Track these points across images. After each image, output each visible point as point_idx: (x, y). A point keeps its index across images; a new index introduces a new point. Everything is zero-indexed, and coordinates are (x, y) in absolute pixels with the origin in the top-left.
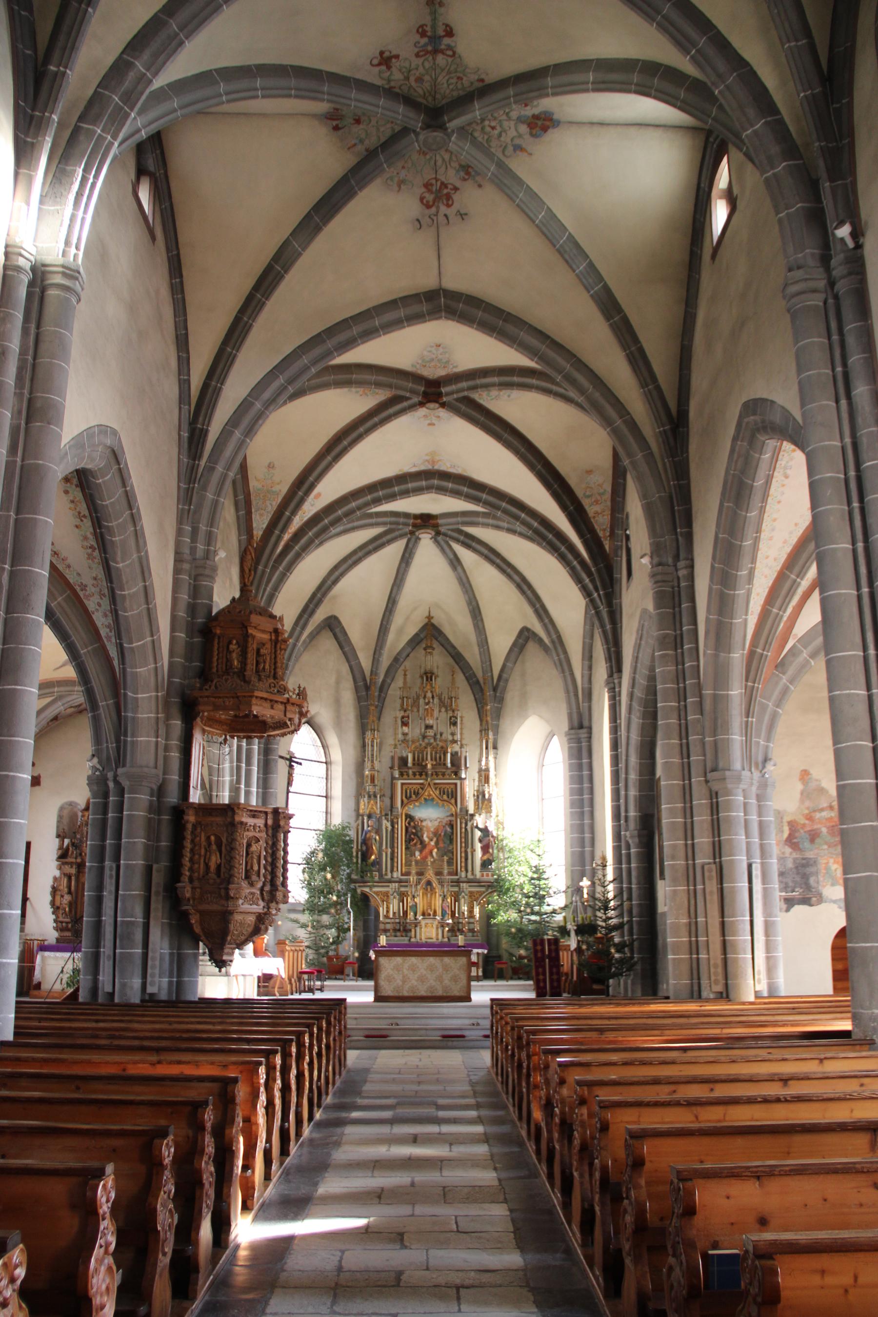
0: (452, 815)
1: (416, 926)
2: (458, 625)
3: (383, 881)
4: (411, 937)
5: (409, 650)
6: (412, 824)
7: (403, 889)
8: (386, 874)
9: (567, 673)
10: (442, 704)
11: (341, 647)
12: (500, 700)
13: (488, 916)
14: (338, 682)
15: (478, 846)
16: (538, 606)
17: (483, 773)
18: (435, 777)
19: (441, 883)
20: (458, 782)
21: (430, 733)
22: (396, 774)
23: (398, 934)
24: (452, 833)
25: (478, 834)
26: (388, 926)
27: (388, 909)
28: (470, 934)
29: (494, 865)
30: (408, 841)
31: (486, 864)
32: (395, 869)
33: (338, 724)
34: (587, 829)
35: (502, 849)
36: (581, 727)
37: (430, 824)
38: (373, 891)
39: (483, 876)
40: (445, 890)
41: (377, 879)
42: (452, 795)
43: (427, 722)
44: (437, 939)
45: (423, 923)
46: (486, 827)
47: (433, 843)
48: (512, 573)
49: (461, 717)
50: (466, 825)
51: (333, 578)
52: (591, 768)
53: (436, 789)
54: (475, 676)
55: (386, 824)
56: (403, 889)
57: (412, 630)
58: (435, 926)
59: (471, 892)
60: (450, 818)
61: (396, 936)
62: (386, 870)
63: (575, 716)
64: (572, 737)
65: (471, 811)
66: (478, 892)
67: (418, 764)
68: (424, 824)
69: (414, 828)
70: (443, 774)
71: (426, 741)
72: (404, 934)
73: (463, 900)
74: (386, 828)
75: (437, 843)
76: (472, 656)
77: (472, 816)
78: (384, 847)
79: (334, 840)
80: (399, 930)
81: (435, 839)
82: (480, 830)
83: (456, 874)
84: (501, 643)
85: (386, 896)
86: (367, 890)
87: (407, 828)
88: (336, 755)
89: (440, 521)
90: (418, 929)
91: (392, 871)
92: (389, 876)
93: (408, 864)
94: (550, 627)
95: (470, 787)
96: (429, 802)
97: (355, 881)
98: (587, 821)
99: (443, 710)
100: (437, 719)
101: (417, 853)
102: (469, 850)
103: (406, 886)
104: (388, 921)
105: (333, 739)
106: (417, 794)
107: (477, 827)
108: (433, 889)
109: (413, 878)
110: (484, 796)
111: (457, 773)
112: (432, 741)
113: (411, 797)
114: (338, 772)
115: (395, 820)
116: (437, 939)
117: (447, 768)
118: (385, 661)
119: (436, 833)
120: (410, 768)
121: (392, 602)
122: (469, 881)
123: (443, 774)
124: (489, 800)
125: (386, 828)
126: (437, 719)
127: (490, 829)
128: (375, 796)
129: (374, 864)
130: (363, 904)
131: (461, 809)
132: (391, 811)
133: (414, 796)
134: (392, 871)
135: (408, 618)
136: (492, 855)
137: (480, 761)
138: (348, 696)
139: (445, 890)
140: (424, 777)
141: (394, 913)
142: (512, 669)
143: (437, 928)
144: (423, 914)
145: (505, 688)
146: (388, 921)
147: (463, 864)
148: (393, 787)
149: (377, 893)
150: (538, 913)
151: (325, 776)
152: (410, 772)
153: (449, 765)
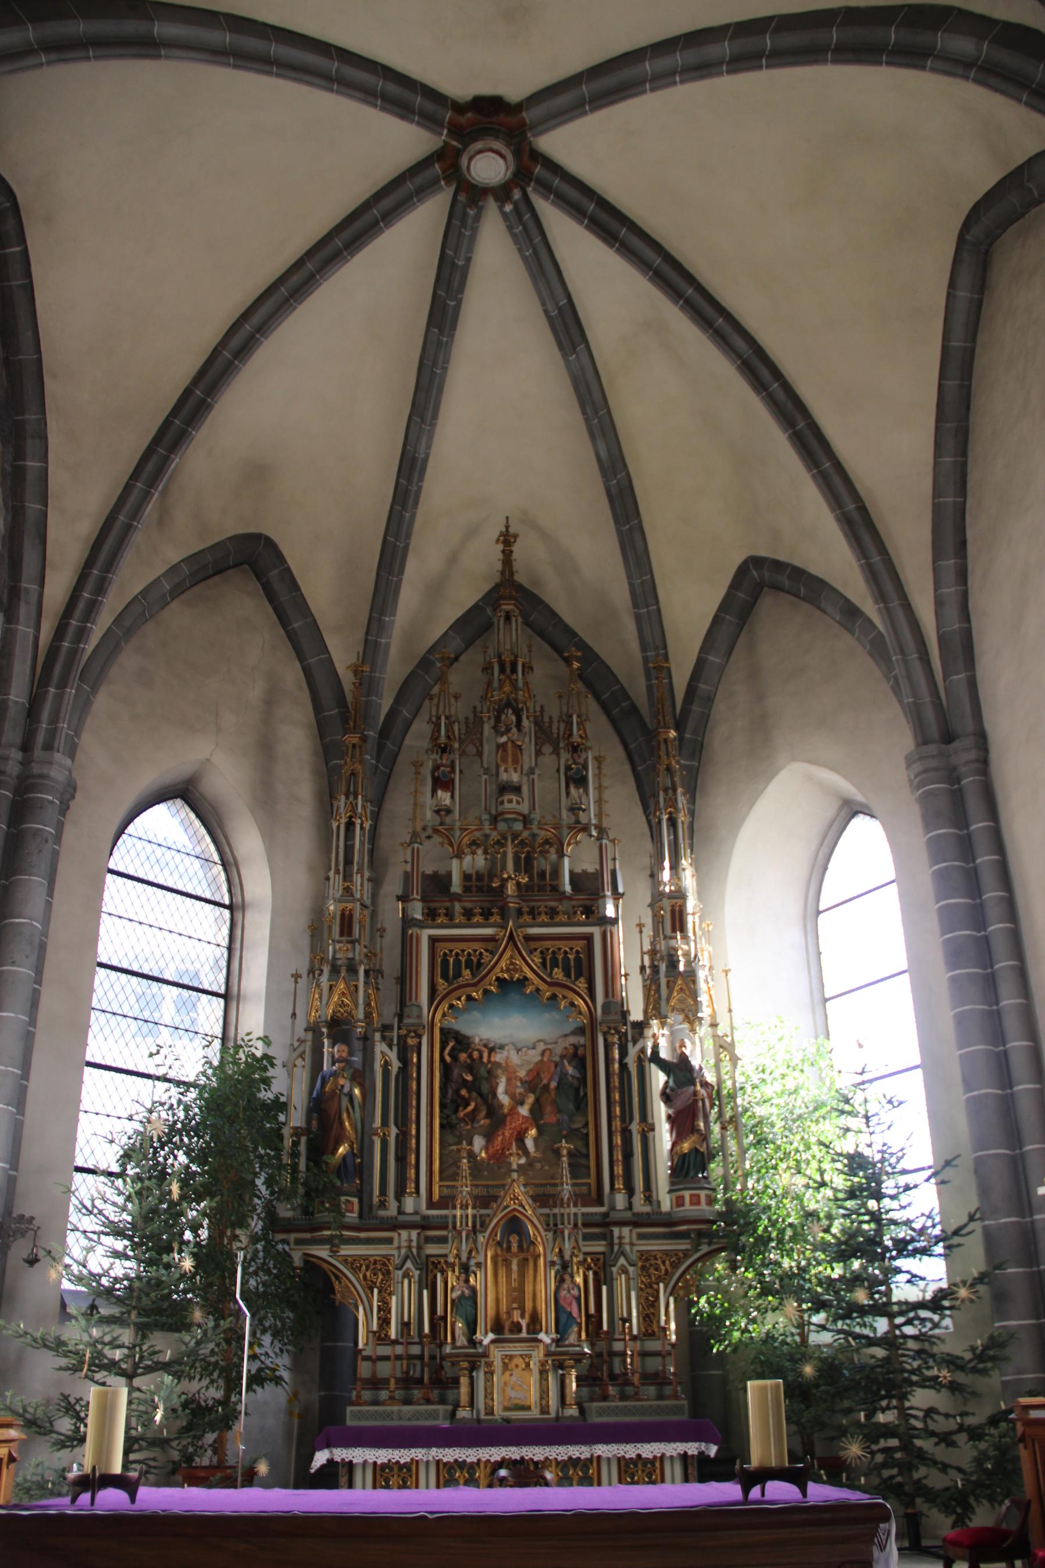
0: (580, 1031)
1: (473, 1367)
2: (578, 571)
3: (372, 1222)
4: (457, 1405)
5: (457, 643)
6: (463, 1056)
7: (432, 1250)
8: (383, 1205)
9: (895, 603)
10: (544, 735)
11: (284, 620)
12: (695, 749)
13: (699, 1334)
14: (270, 701)
15: (661, 1111)
16: (801, 425)
17: (666, 903)
18: (527, 918)
19: (553, 1226)
20: (596, 931)
21: (512, 804)
22: (417, 911)
23: (417, 1393)
24: (583, 1080)
25: (659, 1079)
26: (384, 1369)
27: (382, 1314)
28: (652, 1390)
29: (715, 1168)
30: (451, 1105)
31: (689, 1167)
32: (411, 1187)
33: (266, 801)
34: (1012, 1023)
35: (734, 1120)
36: (948, 737)
37: (515, 1059)
38: (343, 1255)
39: (680, 1202)
40: (568, 1246)
41: (352, 1217)
42: (581, 966)
43: (504, 777)
44: (544, 1410)
45: (496, 1355)
46: (684, 1060)
47: (524, 1111)
48: (728, 330)
49: (599, 759)
50: (624, 1053)
51: (236, 342)
52: (999, 845)
53: (531, 952)
54: (628, 697)
55: (384, 1053)
56: (432, 1250)
57: (464, 596)
58: (534, 1366)
59: (646, 1257)
60: (573, 1040)
61: (407, 1402)
62: (383, 1192)
63: (929, 714)
64: (934, 763)
65: (636, 1014)
66: (666, 1253)
67: (480, 889)
68: (498, 1057)
69: (470, 1068)
70: (553, 913)
71: (502, 826)
72: (435, 1394)
73: (621, 1283)
74: (386, 1065)
75: (537, 1111)
76: (621, 650)
77: (640, 1027)
78: (378, 1122)
79: (232, 1108)
80: (420, 1381)
81: (531, 1099)
82: (664, 1065)
83: (600, 1202)
84: (691, 605)
85: (379, 1276)
86: (322, 1252)
87: (446, 1069)
88: (258, 884)
89: (528, 116)
90: (480, 1376)
91: (400, 1194)
92: (392, 1210)
93: (449, 1171)
94: (837, 481)
95: (628, 952)
96: (514, 996)
97: (288, 1227)
98: (1009, 1001)
99: (547, 749)
100: (532, 771)
101: (478, 1142)
102: (635, 1127)
103: (443, 1240)
104: (384, 1350)
105: (249, 842)
106: (475, 966)
107: (655, 1058)
108: (527, 1245)
109: (462, 1214)
110: (673, 964)
111: (592, 913)
112: (518, 826)
113: (458, 974)
114: (259, 927)
115: (411, 1042)
116: (544, 1410)
117: (562, 897)
118: (394, 670)
119: (533, 1084)
120: (456, 898)
121: (411, 468)
122: (637, 1221)
123: (553, 913)
124: (691, 976)
125: (386, 1065)
126: (532, 771)
127: (695, 1062)
128: (352, 970)
129: (343, 1169)
130: (311, 1306)
131: (606, 1007)
132: (401, 1017)
133: (466, 973)
134: (400, 1194)
135: (453, 559)
136: (705, 1137)
137: (654, 876)
138: (296, 739)
139: (568, 1246)
140: (496, 918)
141: (405, 1326)
142: (722, 669)
143: (543, 1372)
144: (497, 1327)
145: (705, 719)
146: (384, 1350)
147: (619, 1170)
148: (407, 945)
149: (353, 1263)
150: (883, 1309)
151: (225, 943)
152: (458, 907)
153: (568, 888)
